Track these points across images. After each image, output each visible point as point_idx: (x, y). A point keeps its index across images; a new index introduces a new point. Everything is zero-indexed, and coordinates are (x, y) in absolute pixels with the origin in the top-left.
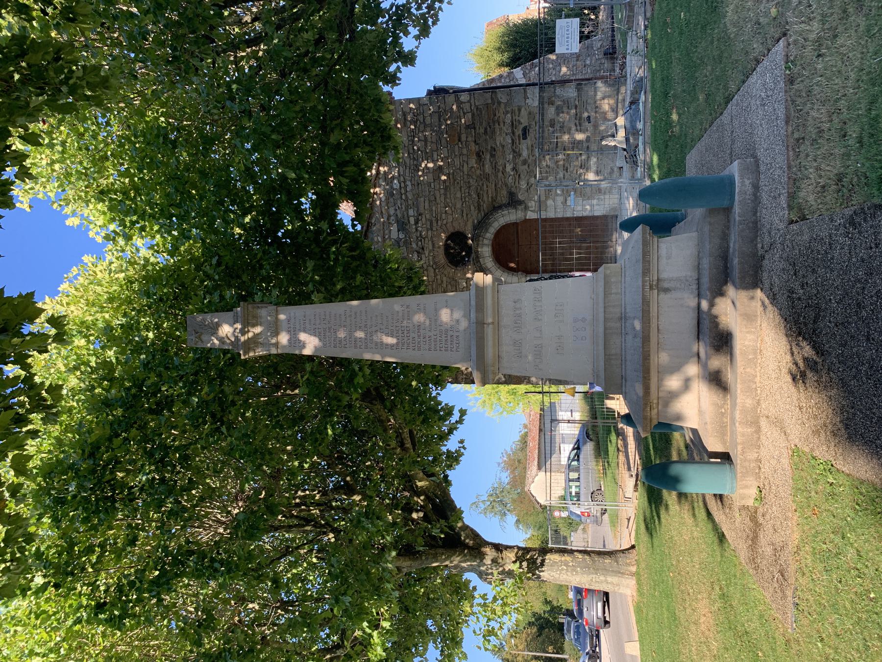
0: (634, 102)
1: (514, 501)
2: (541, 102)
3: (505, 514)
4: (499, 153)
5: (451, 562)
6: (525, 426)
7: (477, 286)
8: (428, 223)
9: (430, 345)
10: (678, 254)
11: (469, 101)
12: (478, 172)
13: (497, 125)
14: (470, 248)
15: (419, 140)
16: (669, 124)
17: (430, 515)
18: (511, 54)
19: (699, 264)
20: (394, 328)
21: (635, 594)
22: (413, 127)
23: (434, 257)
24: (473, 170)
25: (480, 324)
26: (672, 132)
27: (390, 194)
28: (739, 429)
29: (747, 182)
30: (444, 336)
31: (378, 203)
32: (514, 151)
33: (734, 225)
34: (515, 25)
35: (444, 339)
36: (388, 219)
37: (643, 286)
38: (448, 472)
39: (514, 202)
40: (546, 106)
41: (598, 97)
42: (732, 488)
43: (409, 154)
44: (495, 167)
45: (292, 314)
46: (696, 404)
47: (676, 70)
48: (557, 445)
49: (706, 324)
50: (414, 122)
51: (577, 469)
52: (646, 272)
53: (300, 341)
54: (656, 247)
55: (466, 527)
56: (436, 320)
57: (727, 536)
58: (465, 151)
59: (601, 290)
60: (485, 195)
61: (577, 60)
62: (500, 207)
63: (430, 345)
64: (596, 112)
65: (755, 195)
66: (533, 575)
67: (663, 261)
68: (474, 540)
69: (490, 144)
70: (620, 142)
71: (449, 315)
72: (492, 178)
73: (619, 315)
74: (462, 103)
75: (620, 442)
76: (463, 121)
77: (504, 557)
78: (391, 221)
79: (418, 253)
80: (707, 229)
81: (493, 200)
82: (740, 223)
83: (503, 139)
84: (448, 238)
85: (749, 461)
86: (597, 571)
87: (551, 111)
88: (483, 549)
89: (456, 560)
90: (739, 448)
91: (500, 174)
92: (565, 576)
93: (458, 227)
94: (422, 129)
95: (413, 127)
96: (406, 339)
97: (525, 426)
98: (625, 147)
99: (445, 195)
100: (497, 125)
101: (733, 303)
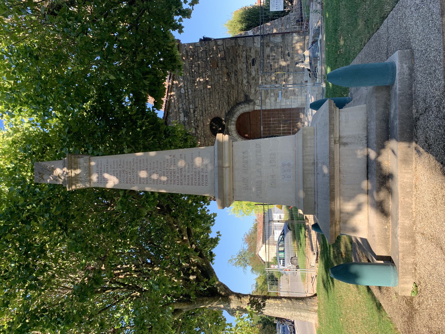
0: (315, 42)
1: (250, 259)
2: (262, 45)
3: (246, 266)
4: (239, 74)
5: (212, 305)
6: (256, 220)
7: (219, 142)
8: (201, 112)
10: (353, 119)
11: (223, 45)
12: (228, 84)
13: (238, 58)
14: (224, 125)
15: (195, 66)
16: (338, 48)
17: (199, 278)
18: (247, 24)
19: (368, 126)
21: (317, 323)
22: (191, 59)
24: (225, 83)
25: (221, 168)
26: (340, 52)
27: (180, 96)
28: (401, 241)
29: (405, 66)
31: (173, 101)
32: (248, 72)
33: (395, 97)
34: (249, 9)
35: (197, 177)
37: (330, 141)
38: (212, 251)
39: (247, 100)
40: (265, 47)
41: (294, 42)
42: (395, 283)
43: (190, 74)
44: (237, 81)
45: (99, 162)
46: (366, 221)
47: (343, 13)
48: (272, 231)
49: (373, 168)
50: (192, 56)
51: (283, 246)
52: (332, 131)
53: (104, 178)
54: (338, 115)
55: (221, 284)
57: (383, 305)
58: (220, 72)
59: (301, 144)
60: (232, 97)
61: (282, 26)
62: (240, 103)
64: (293, 50)
65: (410, 75)
66: (259, 311)
67: (343, 124)
68: (225, 291)
69: (235, 68)
70: (306, 65)
71: (201, 162)
72: (236, 87)
73: (312, 161)
74: (219, 45)
75: (307, 232)
76: (219, 55)
77: (242, 301)
78: (180, 111)
79: (196, 129)
80: (374, 101)
81: (236, 99)
82: (400, 95)
83: (241, 65)
85: (408, 264)
86: (295, 309)
87: (268, 50)
88: (230, 297)
89: (215, 304)
90: (401, 255)
91: (240, 85)
92: (277, 312)
93: (217, 114)
94: (197, 60)
95: (191, 59)
96: (173, 177)
97: (256, 220)
98: (309, 68)
99: (210, 96)
100: (238, 58)
101: (393, 151)
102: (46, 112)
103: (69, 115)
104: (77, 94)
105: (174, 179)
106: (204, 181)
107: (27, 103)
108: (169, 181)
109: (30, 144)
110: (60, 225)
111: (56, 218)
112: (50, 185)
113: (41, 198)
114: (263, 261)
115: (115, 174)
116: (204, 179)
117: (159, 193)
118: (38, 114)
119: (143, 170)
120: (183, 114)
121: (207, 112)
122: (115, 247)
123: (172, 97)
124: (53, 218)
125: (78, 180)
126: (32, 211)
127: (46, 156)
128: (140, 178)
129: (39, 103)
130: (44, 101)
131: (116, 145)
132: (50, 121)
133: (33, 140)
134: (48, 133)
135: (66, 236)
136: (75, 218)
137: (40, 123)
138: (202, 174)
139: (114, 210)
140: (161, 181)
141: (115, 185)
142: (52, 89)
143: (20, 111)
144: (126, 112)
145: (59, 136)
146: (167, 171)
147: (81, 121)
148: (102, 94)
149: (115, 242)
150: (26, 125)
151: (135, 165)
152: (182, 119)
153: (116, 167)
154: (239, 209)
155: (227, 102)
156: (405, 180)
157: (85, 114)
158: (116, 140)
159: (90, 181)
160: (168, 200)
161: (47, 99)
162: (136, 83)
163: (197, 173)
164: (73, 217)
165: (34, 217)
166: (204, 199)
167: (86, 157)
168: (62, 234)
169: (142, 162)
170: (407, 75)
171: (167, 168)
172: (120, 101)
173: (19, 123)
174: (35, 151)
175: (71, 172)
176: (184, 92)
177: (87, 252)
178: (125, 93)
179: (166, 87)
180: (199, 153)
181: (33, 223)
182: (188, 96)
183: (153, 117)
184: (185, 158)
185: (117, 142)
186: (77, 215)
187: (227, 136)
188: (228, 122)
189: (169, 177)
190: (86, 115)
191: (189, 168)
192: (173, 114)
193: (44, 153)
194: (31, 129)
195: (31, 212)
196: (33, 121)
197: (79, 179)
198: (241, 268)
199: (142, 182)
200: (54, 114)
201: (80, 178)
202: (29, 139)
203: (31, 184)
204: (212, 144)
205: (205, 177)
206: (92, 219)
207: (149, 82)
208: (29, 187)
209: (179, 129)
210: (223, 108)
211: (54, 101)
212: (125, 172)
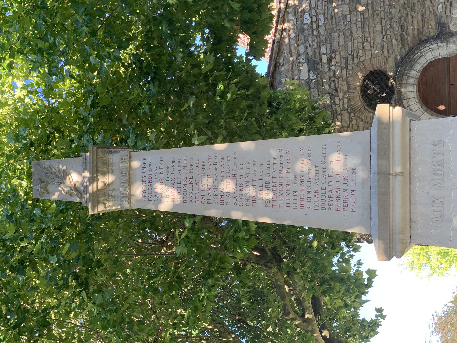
7: (380, 122)
8: (343, 61)
9: (316, 202)
20: (270, 179)
23: (349, 100)
25: (384, 175)
27: (300, 30)
30: (335, 190)
31: (287, 40)
35: (335, 194)
36: (297, 58)
39: (443, 34)
45: (148, 161)
56: (324, 169)
62: (428, 40)
63: (316, 202)
78: (301, 60)
79: (331, 95)
84: (366, 77)
93: (376, 65)
96: (285, 193)
99: (363, 28)
102: (54, 67)
103: (93, 72)
104: (108, 33)
105: (288, 197)
106: (349, 202)
107: (22, 53)
108: (278, 201)
109: (26, 128)
110: (77, 277)
111: (69, 264)
112: (58, 203)
113: (44, 226)
115: (176, 184)
116: (349, 198)
117: (257, 223)
118: (40, 72)
119: (228, 178)
120: (306, 65)
121: (356, 60)
122: (174, 324)
123: (285, 34)
124: (65, 264)
125: (108, 195)
126: (28, 251)
127: (51, 150)
128: (222, 194)
129: (43, 53)
130: (50, 48)
131: (177, 129)
132: (60, 85)
133: (31, 119)
134: (57, 107)
135: (86, 299)
136: (103, 265)
137: (43, 88)
138: (345, 187)
139: (172, 253)
140: (261, 200)
141: (175, 206)
142: (64, 25)
143: (10, 66)
144: (197, 65)
145: (76, 112)
146: (274, 180)
147: (113, 83)
148: (152, 32)
149: (174, 315)
150: (19, 93)
151: (213, 167)
152: (304, 75)
153: (176, 171)
154: (424, 262)
155: (399, 38)
157: (122, 70)
158: (178, 120)
159: (130, 197)
160: (275, 239)
161: (54, 43)
162: (217, 8)
163: (334, 185)
164: (99, 263)
165: (30, 261)
166: (347, 237)
167: (124, 152)
168: (80, 294)
169: (225, 161)
171: (275, 174)
172: (186, 44)
173: (7, 90)
174: (35, 140)
176: (309, 22)
177: (123, 330)
178: (195, 29)
179: (274, 13)
180: (339, 144)
181: (29, 271)
182: (317, 29)
183: (247, 73)
184: (309, 155)
185: (178, 123)
186: (106, 261)
187: (398, 109)
188: (402, 79)
189: (277, 192)
190: (124, 73)
191: (317, 176)
192: (286, 66)
193: (50, 144)
194: (27, 100)
195: (25, 252)
196: (32, 85)
197: (110, 192)
199: (225, 202)
200: (68, 70)
201: (114, 190)
202: (25, 120)
203: (26, 200)
204: (366, 126)
205: (349, 194)
206: (133, 270)
207: (239, 5)
208: (23, 206)
209: (299, 97)
210: (391, 51)
211: (67, 46)
212: (193, 182)
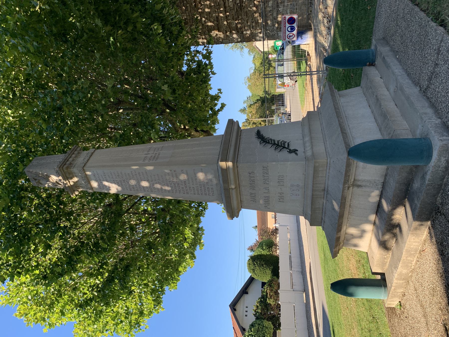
29: (443, 159)
30: (203, 187)
56: (196, 179)
73: (323, 188)
82: (428, 185)
114: (260, 51)
125: (78, 186)
156: (412, 247)
170: (442, 168)
175: (69, 182)
198: (238, 51)
